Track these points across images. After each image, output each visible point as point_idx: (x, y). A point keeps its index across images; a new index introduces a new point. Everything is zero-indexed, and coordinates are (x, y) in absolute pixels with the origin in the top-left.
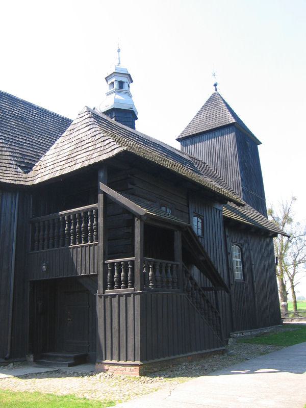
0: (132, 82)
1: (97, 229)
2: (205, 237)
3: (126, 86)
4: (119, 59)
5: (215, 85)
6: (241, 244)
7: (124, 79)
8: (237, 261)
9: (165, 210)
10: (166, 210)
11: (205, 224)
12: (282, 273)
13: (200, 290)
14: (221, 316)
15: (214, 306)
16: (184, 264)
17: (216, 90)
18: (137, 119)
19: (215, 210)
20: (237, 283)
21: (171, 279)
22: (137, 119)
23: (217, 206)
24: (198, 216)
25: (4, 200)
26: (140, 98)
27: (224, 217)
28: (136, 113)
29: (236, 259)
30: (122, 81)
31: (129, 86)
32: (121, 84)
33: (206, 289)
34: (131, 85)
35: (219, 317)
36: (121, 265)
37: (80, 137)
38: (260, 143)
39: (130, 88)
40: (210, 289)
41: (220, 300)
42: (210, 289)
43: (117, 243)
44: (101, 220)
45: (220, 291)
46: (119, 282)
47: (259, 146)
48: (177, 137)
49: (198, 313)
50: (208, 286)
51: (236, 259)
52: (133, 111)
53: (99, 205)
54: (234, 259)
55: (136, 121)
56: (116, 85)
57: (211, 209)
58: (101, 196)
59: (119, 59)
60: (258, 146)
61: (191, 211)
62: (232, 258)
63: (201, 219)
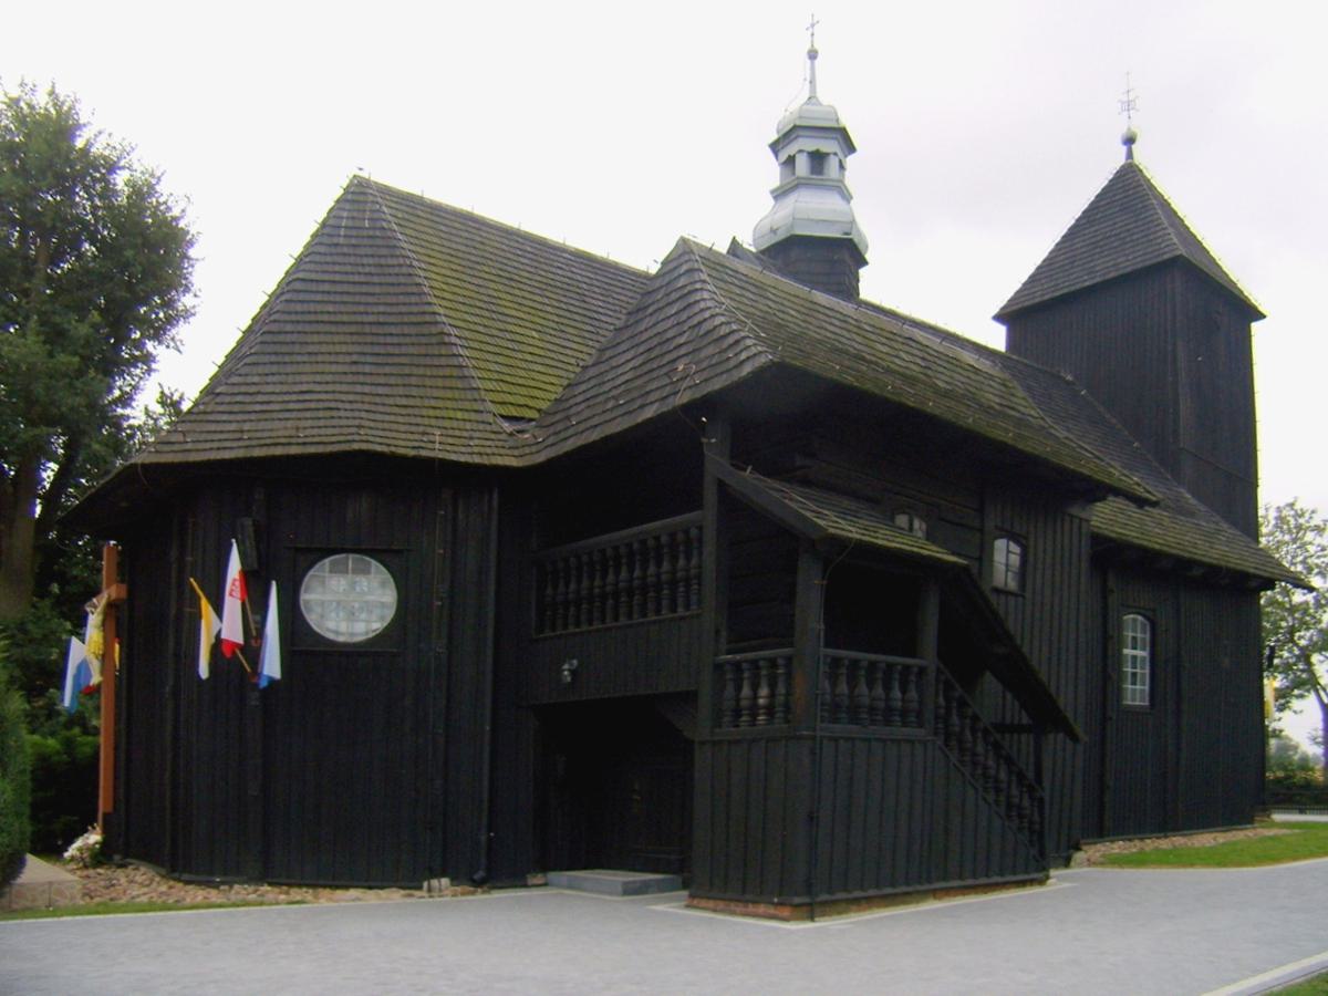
0: (851, 149)
1: (699, 577)
2: (1028, 594)
3: (833, 163)
4: (812, 82)
5: (1130, 141)
6: (1154, 610)
7: (827, 146)
8: (1134, 658)
9: (906, 526)
10: (911, 525)
11: (1031, 559)
12: (948, 709)
13: (986, 732)
14: (1047, 799)
15: (1030, 775)
16: (942, 666)
17: (1130, 155)
18: (865, 263)
19: (1067, 518)
20: (1134, 712)
21: (900, 704)
22: (865, 263)
23: (1075, 510)
24: (1012, 536)
25: (461, 509)
26: (871, 204)
27: (1097, 539)
28: (861, 247)
29: (1135, 655)
30: (813, 148)
31: (842, 167)
32: (818, 159)
33: (1002, 727)
34: (850, 161)
35: (1041, 800)
36: (758, 668)
37: (660, 328)
38: (1260, 316)
39: (847, 173)
40: (1018, 729)
41: (1047, 763)
42: (1018, 729)
43: (756, 609)
44: (710, 549)
45: (1051, 736)
46: (737, 713)
47: (1255, 326)
48: (995, 310)
49: (976, 789)
50: (1008, 721)
51: (1135, 655)
52: (851, 240)
53: (707, 516)
54: (1127, 651)
55: (863, 272)
56: (802, 166)
57: (1063, 520)
58: (710, 495)
59: (812, 82)
60: (1255, 326)
61: (990, 525)
62: (1121, 644)
63: (1018, 542)
